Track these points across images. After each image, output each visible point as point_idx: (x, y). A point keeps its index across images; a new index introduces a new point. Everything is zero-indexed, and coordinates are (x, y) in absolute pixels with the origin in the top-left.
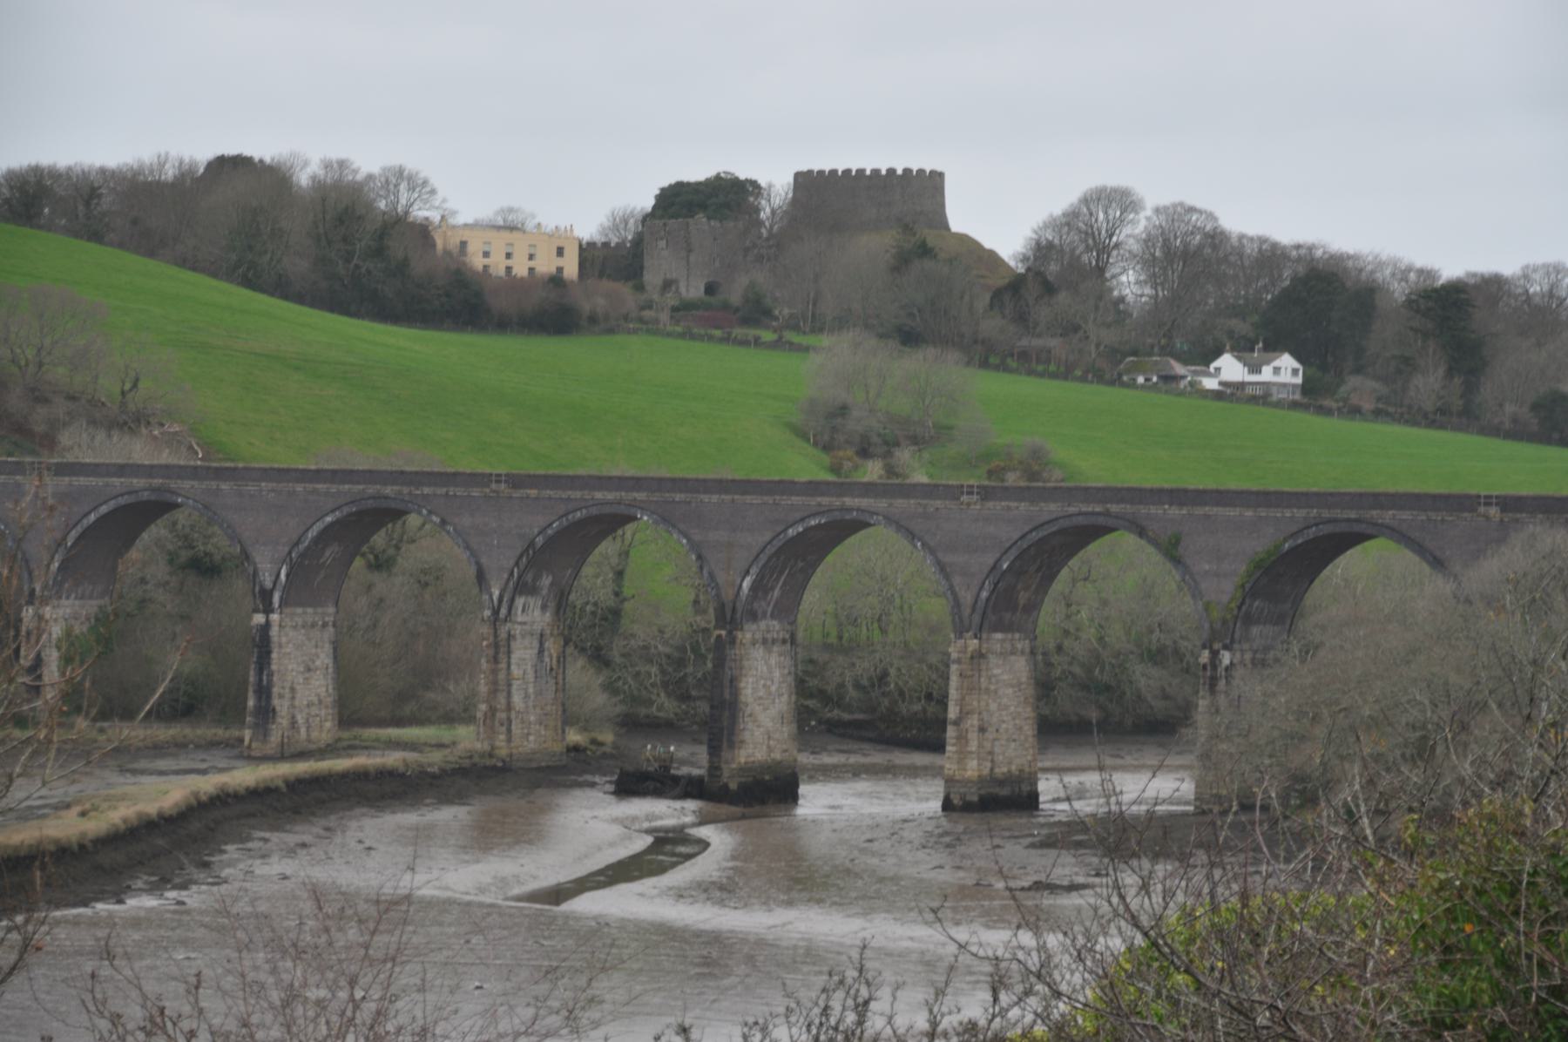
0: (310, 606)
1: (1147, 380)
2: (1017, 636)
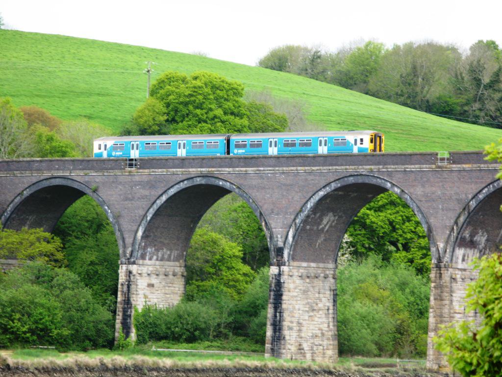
0: (313, 261)
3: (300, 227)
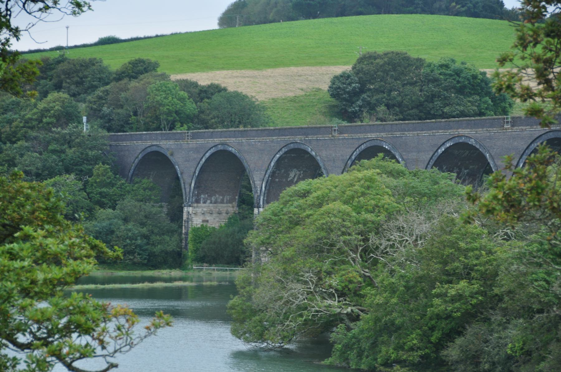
3: (269, 181)
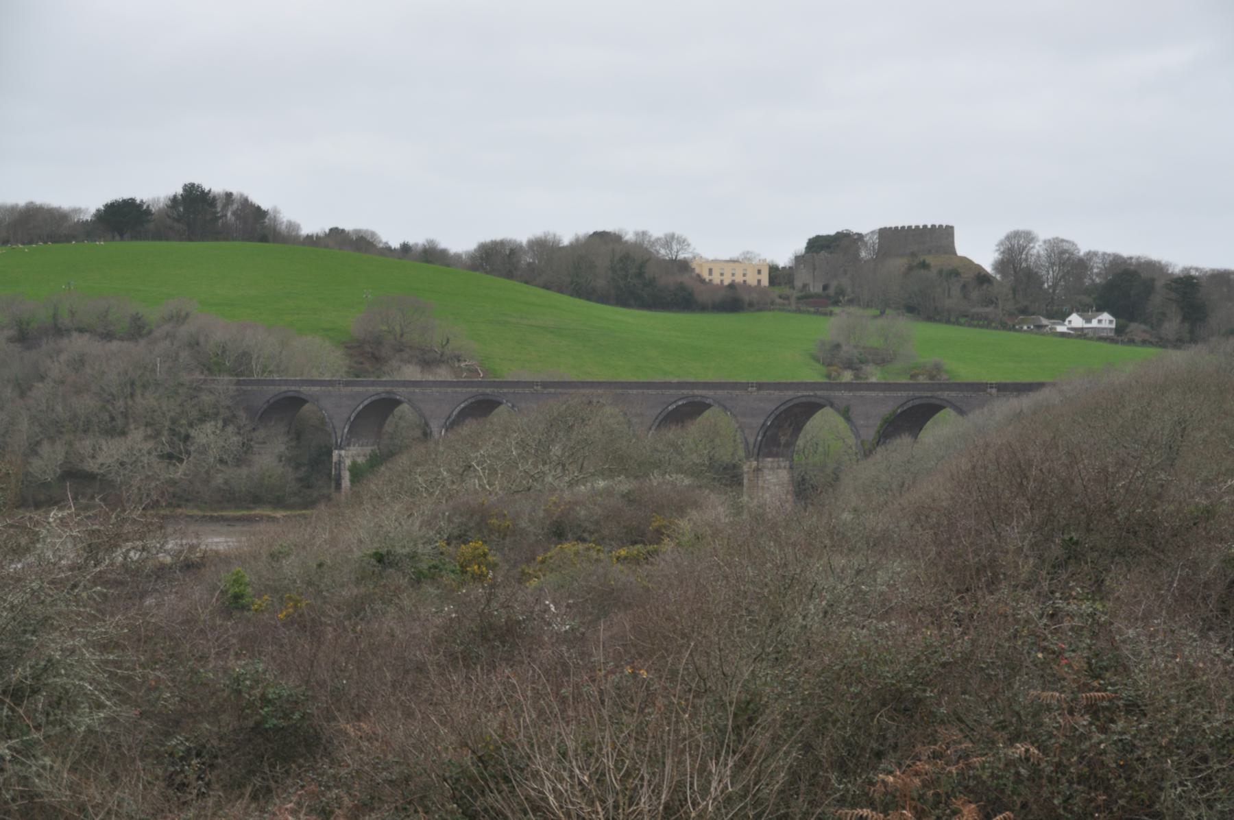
1: (1028, 328)
2: (781, 459)
